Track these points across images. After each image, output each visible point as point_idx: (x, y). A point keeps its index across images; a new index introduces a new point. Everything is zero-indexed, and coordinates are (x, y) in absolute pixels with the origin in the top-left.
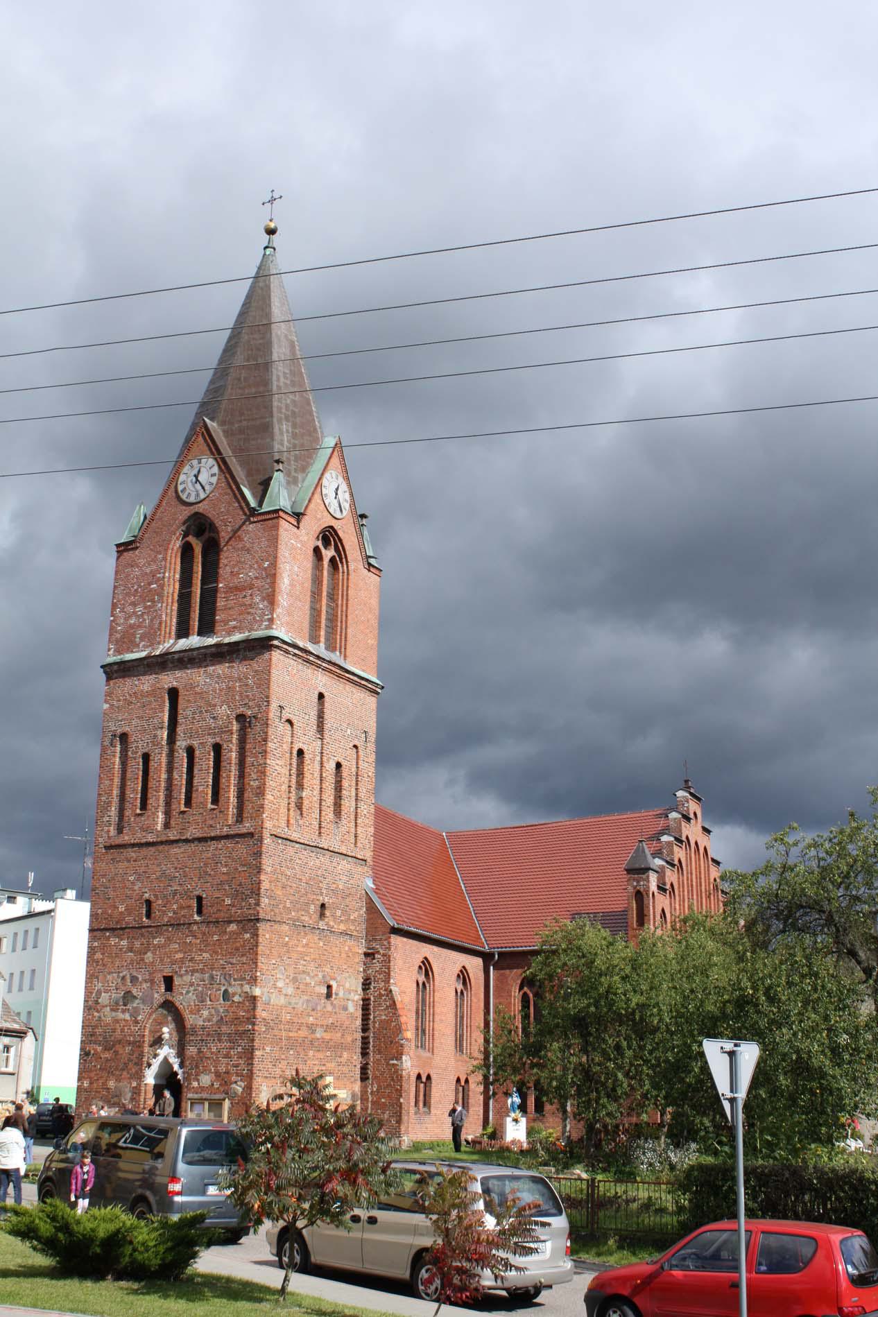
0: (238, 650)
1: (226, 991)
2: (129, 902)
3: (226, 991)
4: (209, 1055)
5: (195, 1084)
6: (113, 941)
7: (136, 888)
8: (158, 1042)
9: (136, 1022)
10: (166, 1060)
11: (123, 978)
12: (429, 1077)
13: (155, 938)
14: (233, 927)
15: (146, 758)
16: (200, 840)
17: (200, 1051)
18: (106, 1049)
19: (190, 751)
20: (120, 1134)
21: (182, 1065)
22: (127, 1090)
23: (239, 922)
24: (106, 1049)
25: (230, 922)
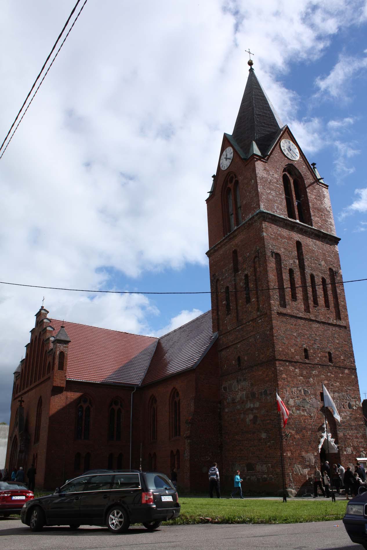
0: (326, 238)
1: (349, 403)
2: (297, 348)
3: (349, 403)
4: (348, 437)
5: (345, 453)
6: (291, 368)
7: (298, 340)
8: (322, 429)
9: (311, 417)
10: (326, 441)
11: (300, 391)
12: (178, 451)
13: (313, 370)
14: (346, 371)
15: (291, 272)
16: (324, 323)
17: (344, 435)
18: (297, 433)
19: (312, 277)
20: (24, 488)
21: (336, 442)
22: (313, 457)
23: (349, 369)
24: (297, 433)
25: (346, 368)
